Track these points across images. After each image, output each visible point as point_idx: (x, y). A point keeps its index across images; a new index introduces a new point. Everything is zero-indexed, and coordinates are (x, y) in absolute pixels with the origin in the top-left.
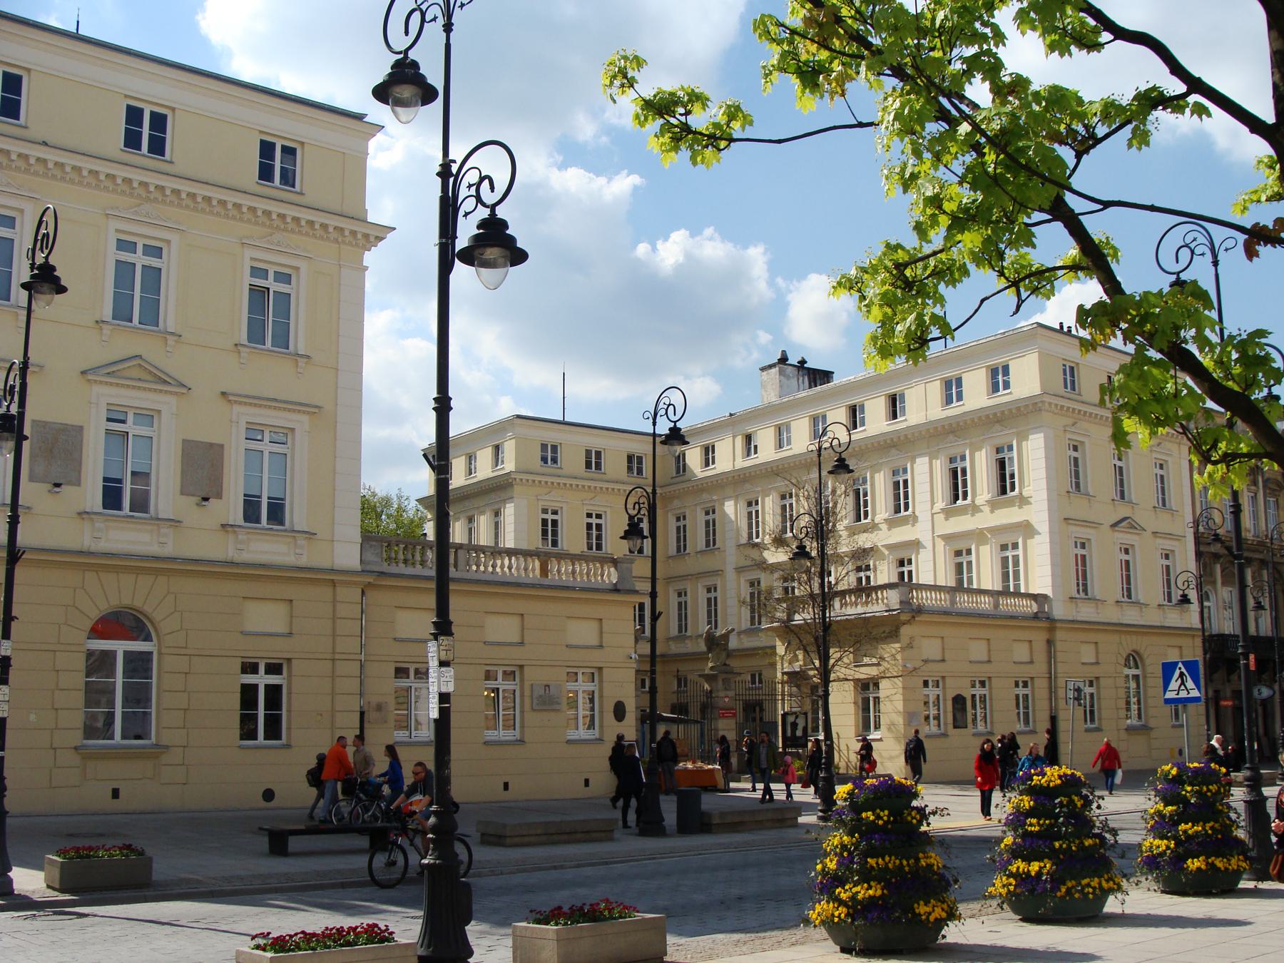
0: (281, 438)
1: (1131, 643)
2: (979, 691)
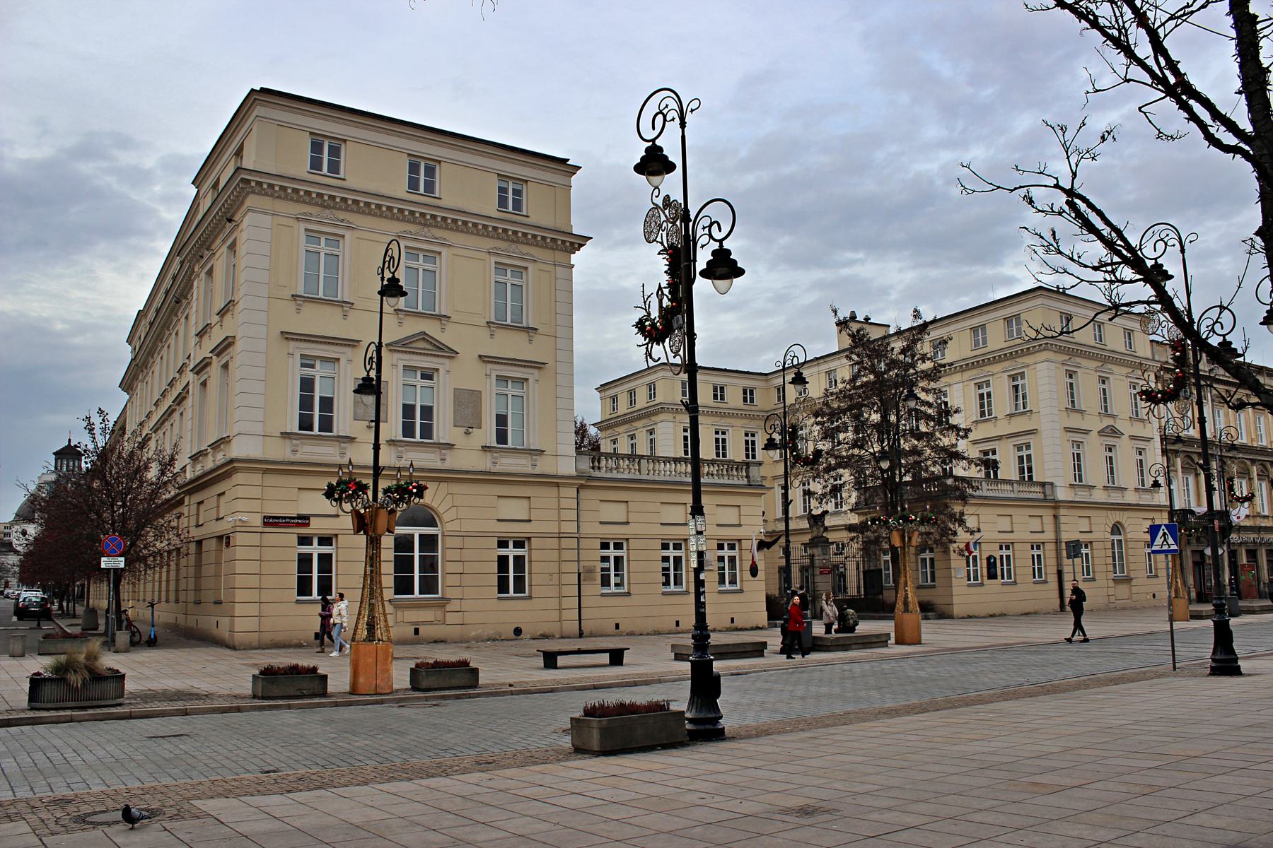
1: (1115, 516)
2: (1004, 553)
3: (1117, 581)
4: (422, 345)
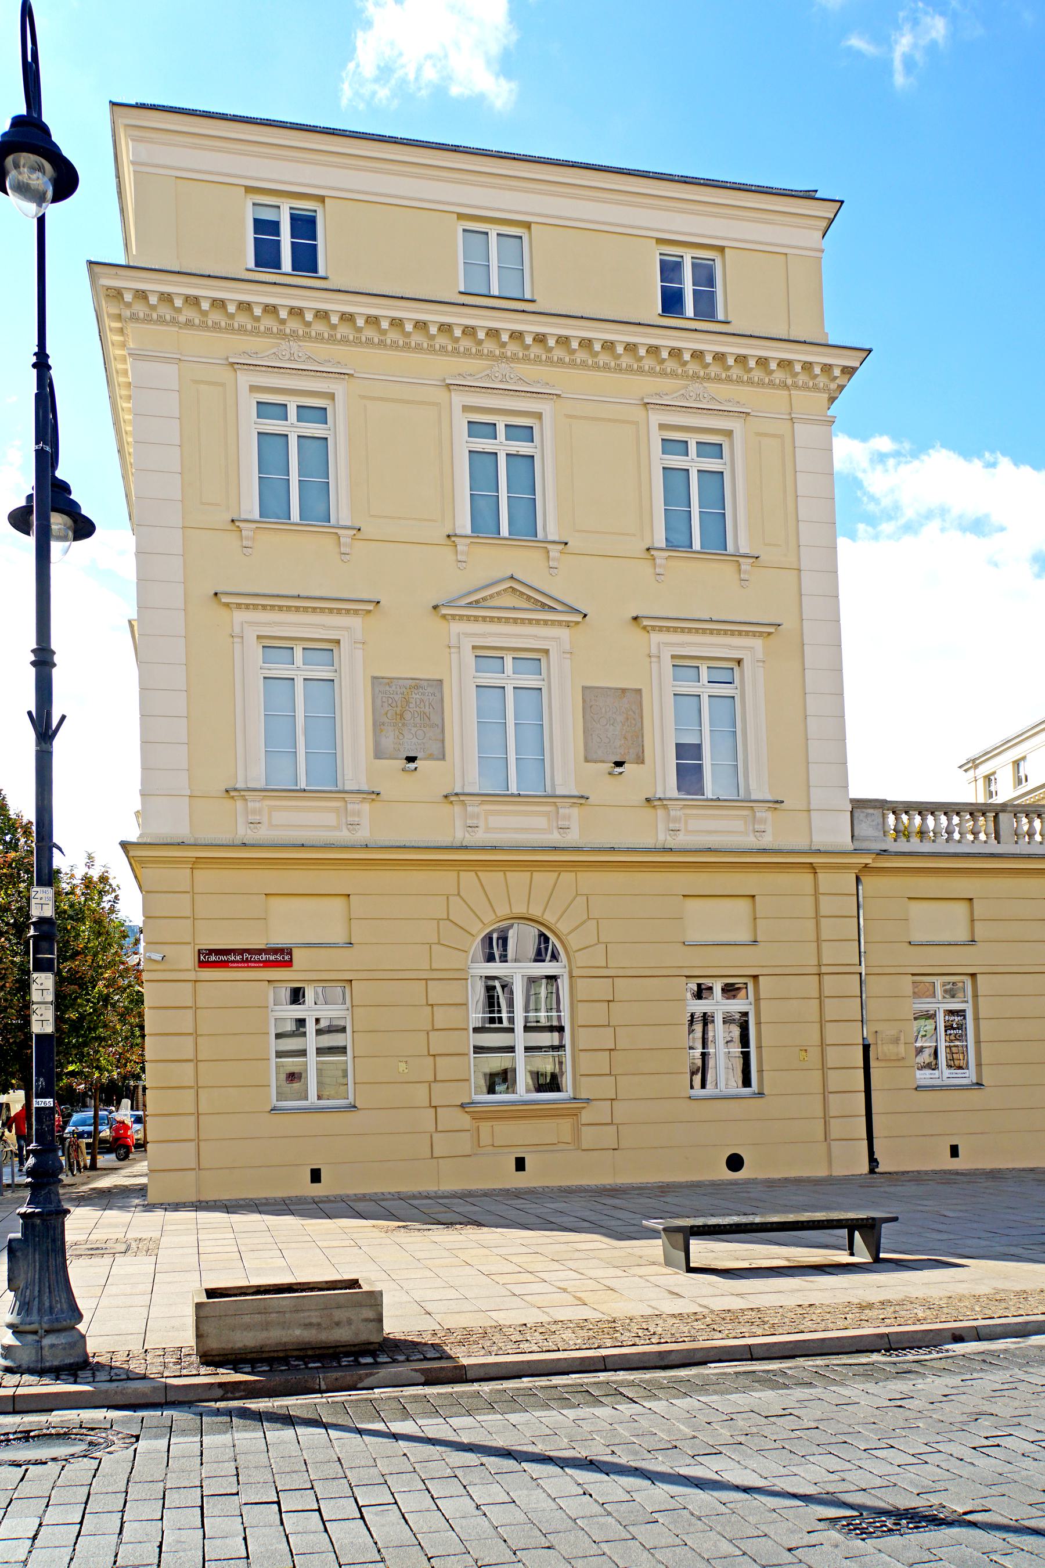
0: (725, 676)
3: (692, 1016)
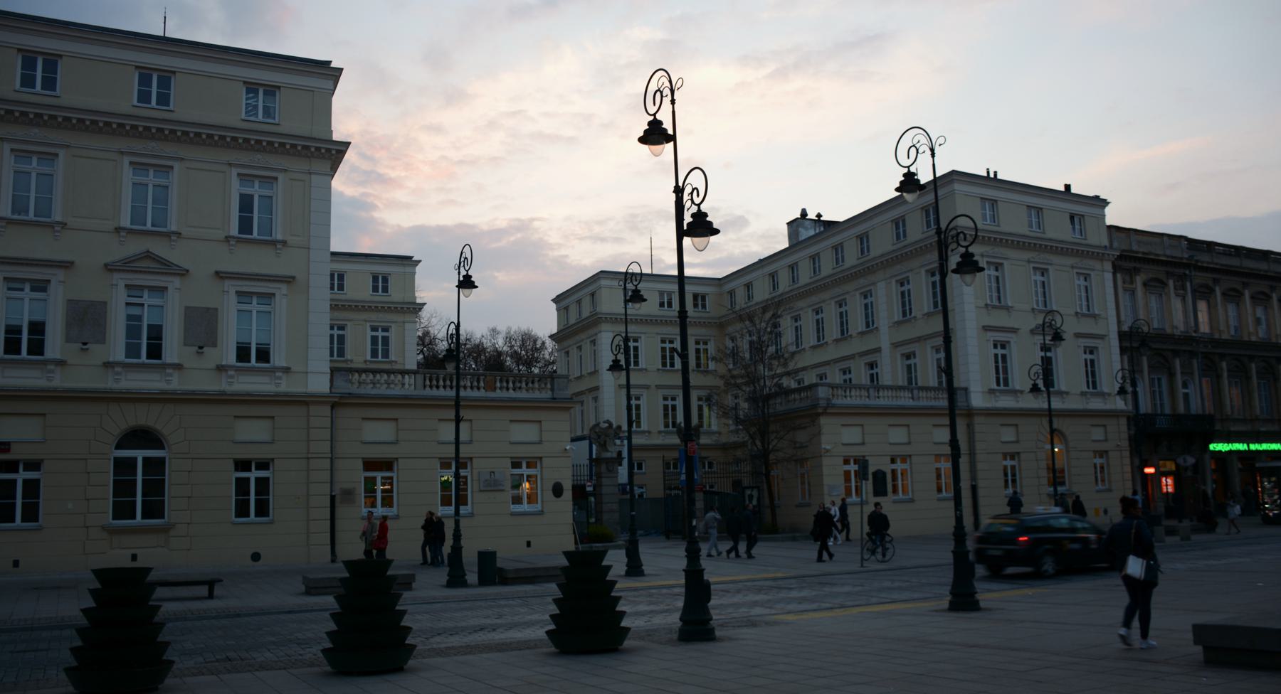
4: (145, 264)
